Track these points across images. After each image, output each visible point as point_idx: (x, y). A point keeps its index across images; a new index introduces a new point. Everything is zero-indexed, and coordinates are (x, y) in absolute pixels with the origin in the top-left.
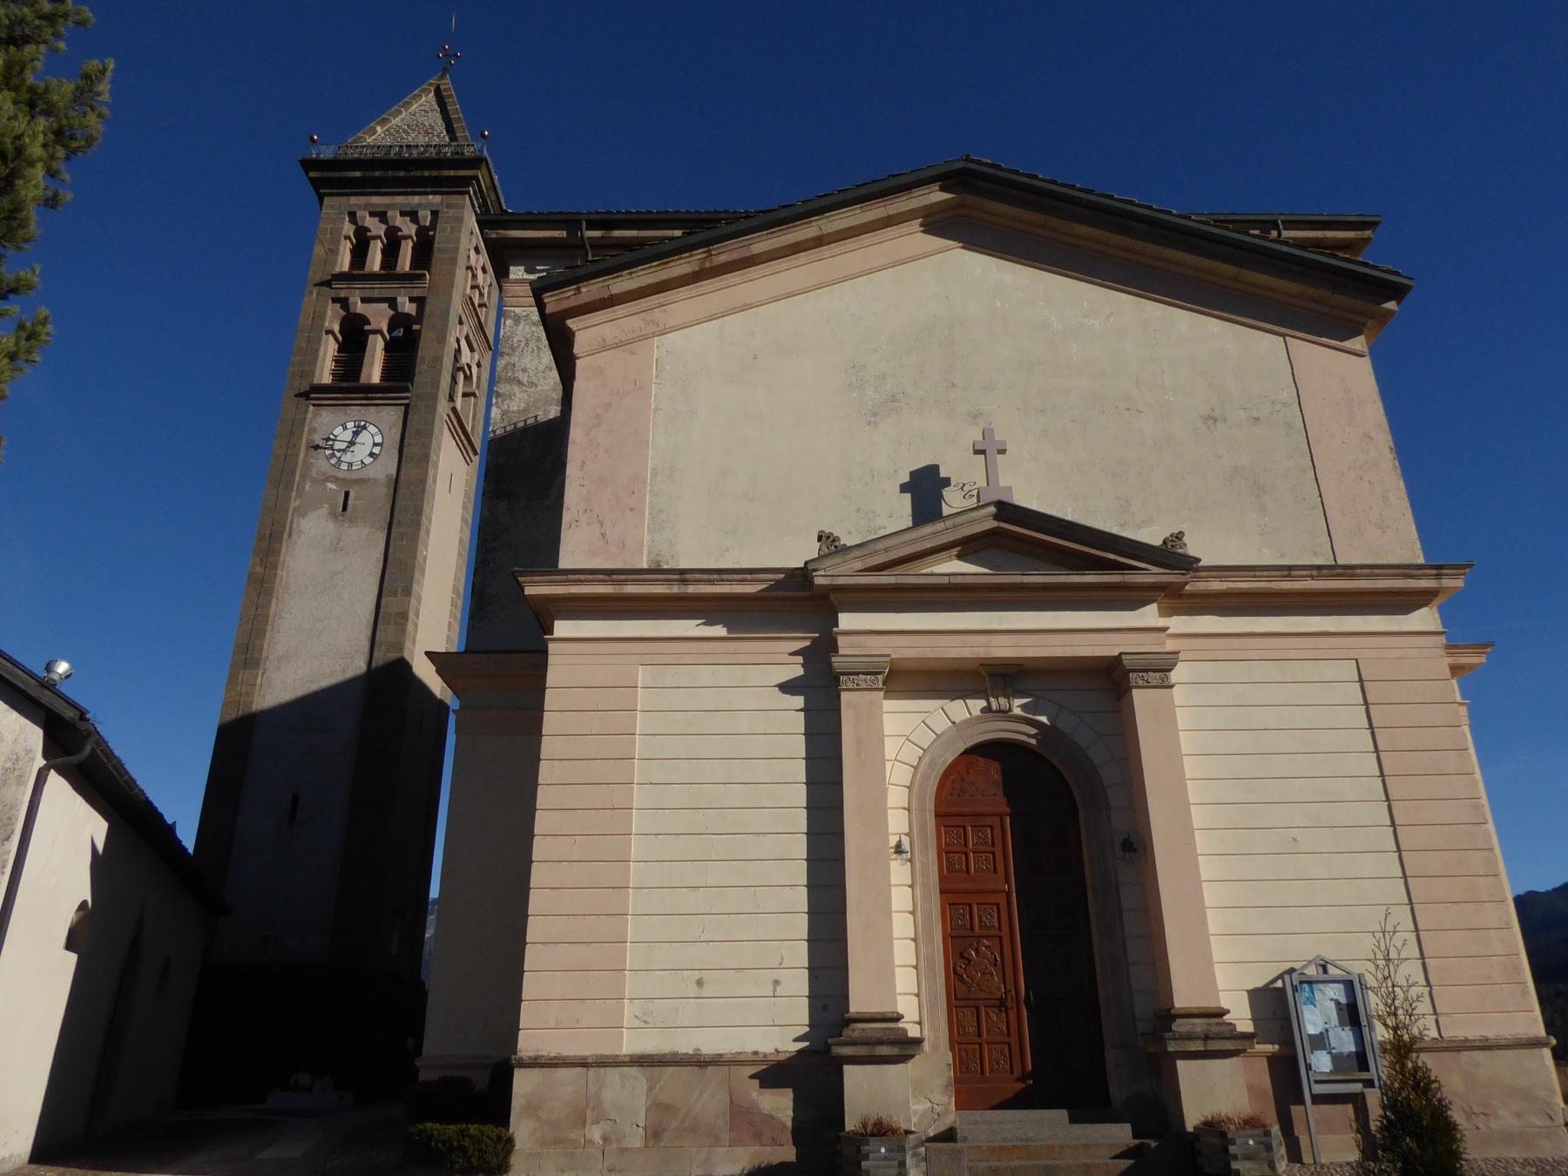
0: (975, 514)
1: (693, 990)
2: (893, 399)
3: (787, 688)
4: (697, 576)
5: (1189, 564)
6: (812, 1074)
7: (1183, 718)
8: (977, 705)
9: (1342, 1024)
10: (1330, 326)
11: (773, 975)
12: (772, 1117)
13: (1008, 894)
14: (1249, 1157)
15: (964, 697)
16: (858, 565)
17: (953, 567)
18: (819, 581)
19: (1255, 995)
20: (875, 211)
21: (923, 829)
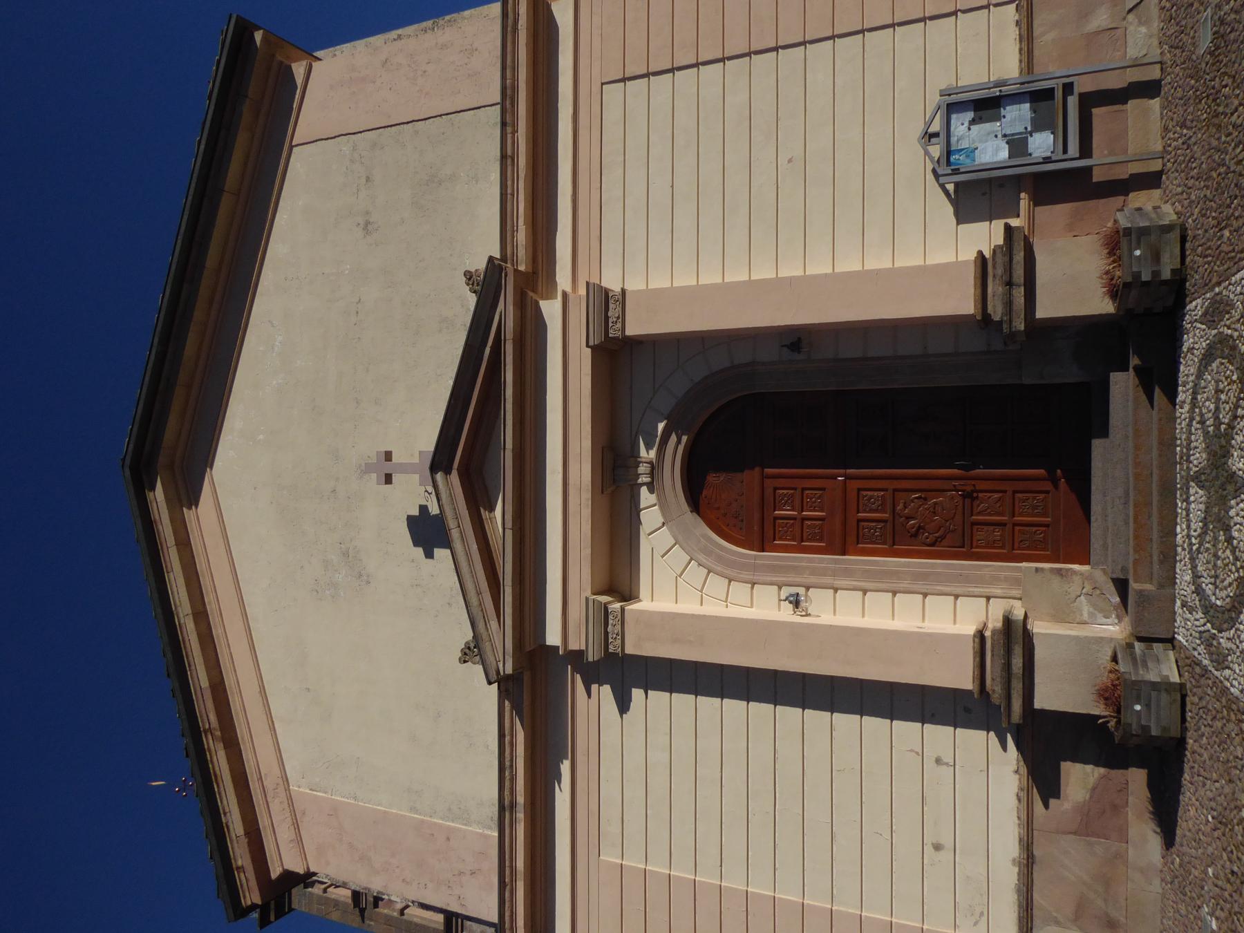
0: (444, 496)
1: (946, 856)
2: (346, 554)
3: (623, 705)
4: (507, 792)
5: (495, 269)
6: (1046, 745)
7: (659, 282)
8: (646, 497)
9: (998, 118)
10: (281, 101)
11: (929, 764)
12: (1094, 789)
13: (847, 477)
14: (1156, 257)
15: (638, 511)
16: (494, 624)
17: (499, 517)
18: (509, 670)
19: (963, 216)
20: (172, 557)
21: (773, 569)
